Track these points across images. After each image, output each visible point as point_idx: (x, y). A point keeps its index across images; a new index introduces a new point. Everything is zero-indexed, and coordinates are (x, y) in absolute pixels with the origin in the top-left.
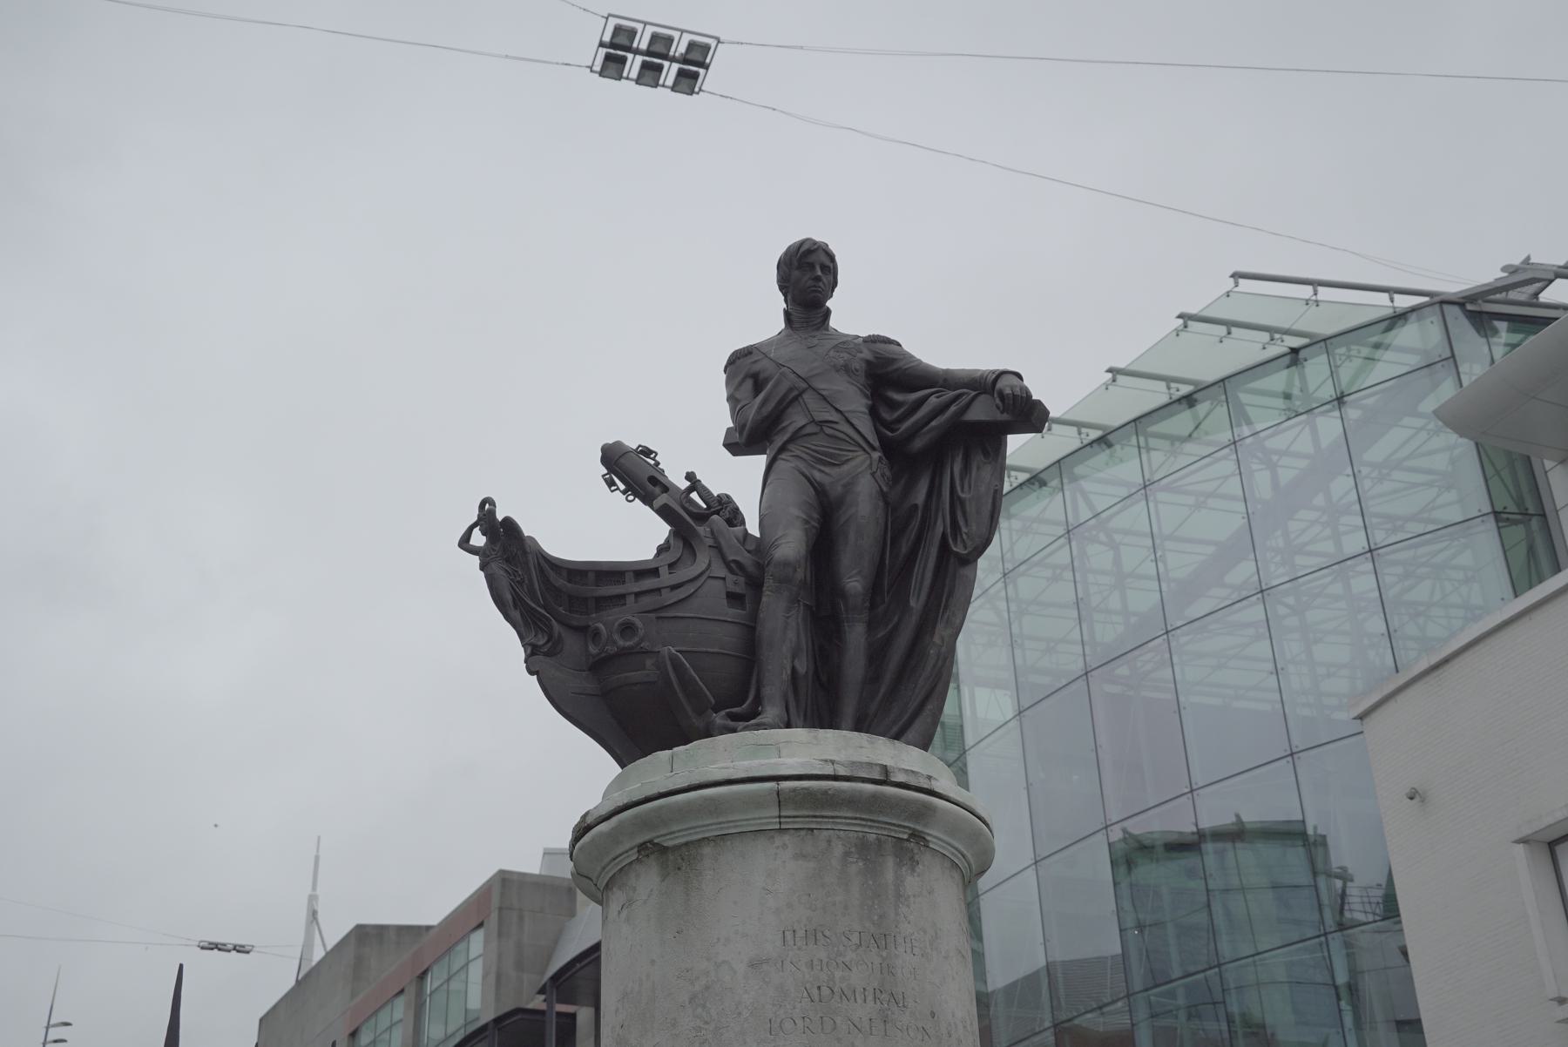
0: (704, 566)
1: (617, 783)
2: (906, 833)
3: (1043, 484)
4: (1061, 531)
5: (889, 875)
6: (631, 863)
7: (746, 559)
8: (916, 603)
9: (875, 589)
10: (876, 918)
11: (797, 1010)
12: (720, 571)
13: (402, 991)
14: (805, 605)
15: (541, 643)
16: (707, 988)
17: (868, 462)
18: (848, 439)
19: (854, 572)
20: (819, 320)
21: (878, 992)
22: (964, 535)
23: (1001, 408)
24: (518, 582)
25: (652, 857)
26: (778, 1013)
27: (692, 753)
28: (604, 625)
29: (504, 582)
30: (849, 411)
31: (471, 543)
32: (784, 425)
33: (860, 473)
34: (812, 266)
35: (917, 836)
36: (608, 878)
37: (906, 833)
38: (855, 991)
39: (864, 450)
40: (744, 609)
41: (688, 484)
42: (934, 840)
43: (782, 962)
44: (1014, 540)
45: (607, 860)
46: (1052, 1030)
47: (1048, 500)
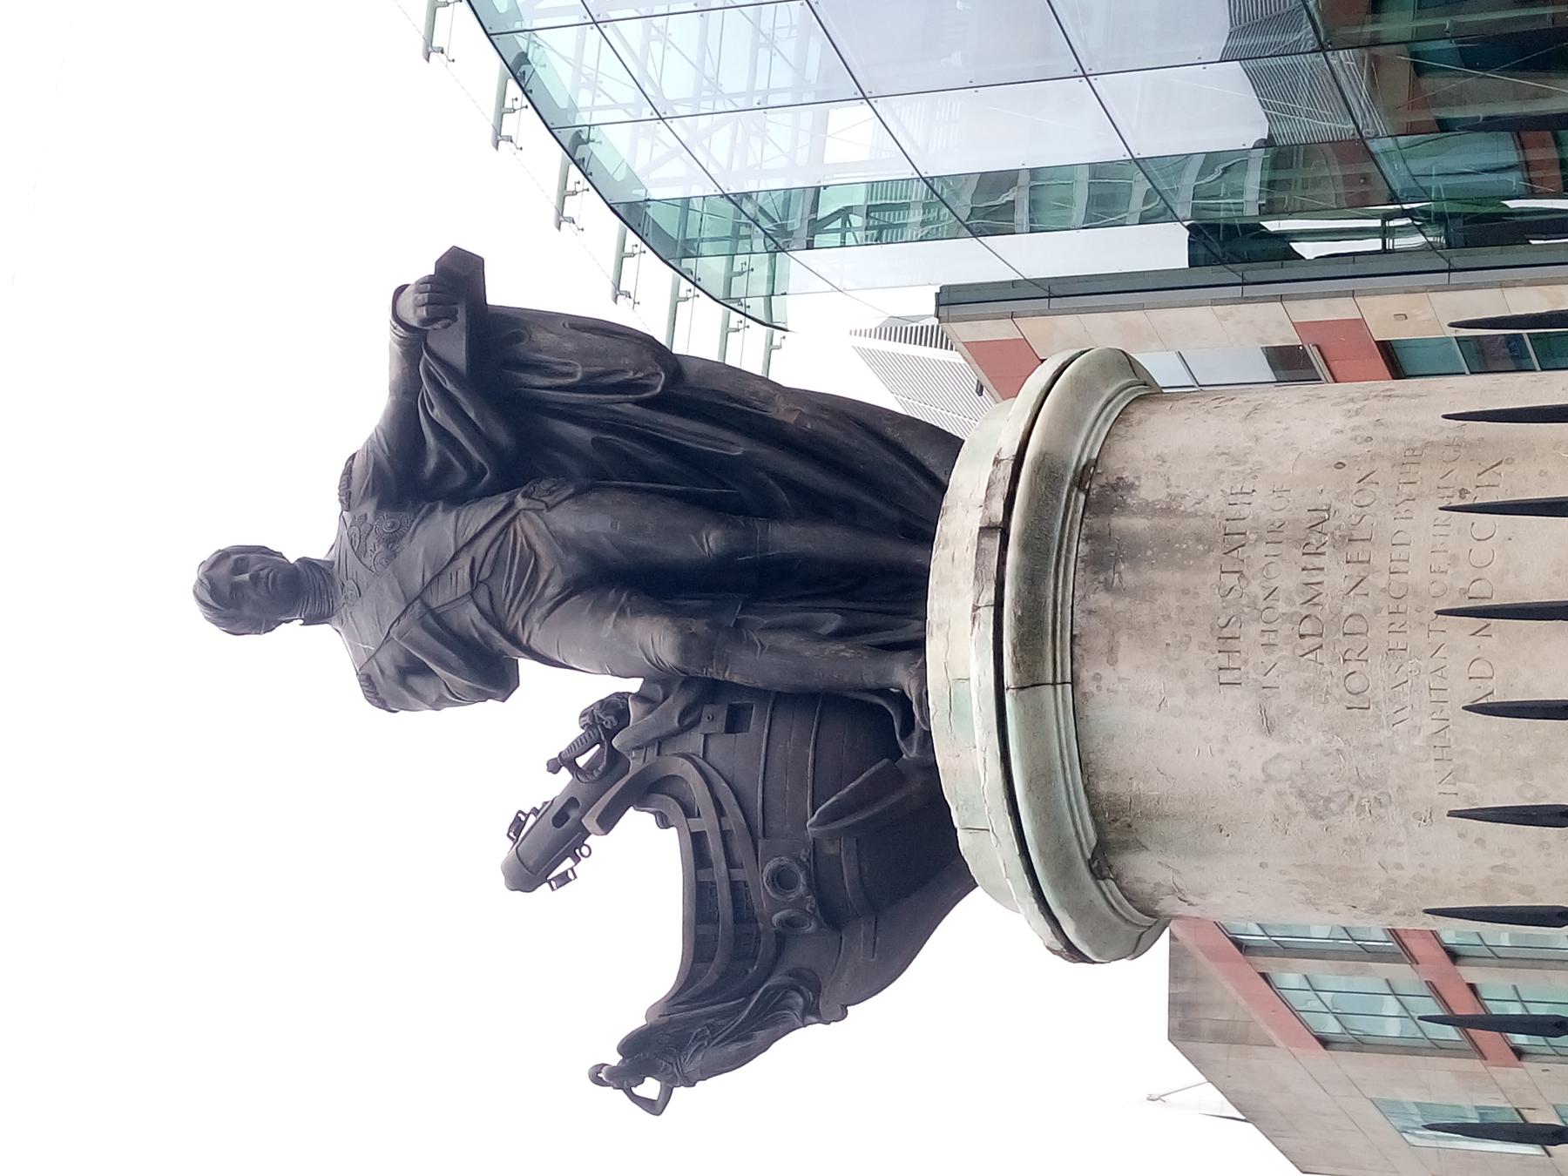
0: (688, 765)
1: (999, 895)
2: (1077, 497)
3: (523, 58)
4: (593, 34)
5: (1138, 524)
6: (1121, 889)
7: (675, 705)
8: (738, 447)
9: (717, 508)
10: (1200, 547)
11: (1334, 670)
12: (695, 741)
13: (1264, 976)
14: (742, 611)
15: (800, 1000)
16: (1301, 795)
17: (533, 516)
18: (498, 544)
20: (318, 576)
21: (1308, 549)
22: (639, 375)
23: (448, 321)
25: (1112, 861)
26: (1337, 697)
27: (961, 803)
28: (774, 914)
29: (715, 1054)
30: (456, 541)
31: (656, 1098)
32: (477, 636)
33: (547, 526)
34: (236, 587)
35: (1082, 479)
36: (1141, 915)
37: (1077, 496)
38: (1306, 584)
39: (513, 519)
41: (564, 770)
42: (1087, 450)
43: (1264, 688)
44: (610, 102)
45: (1115, 919)
46: (1329, 54)
47: (548, 52)
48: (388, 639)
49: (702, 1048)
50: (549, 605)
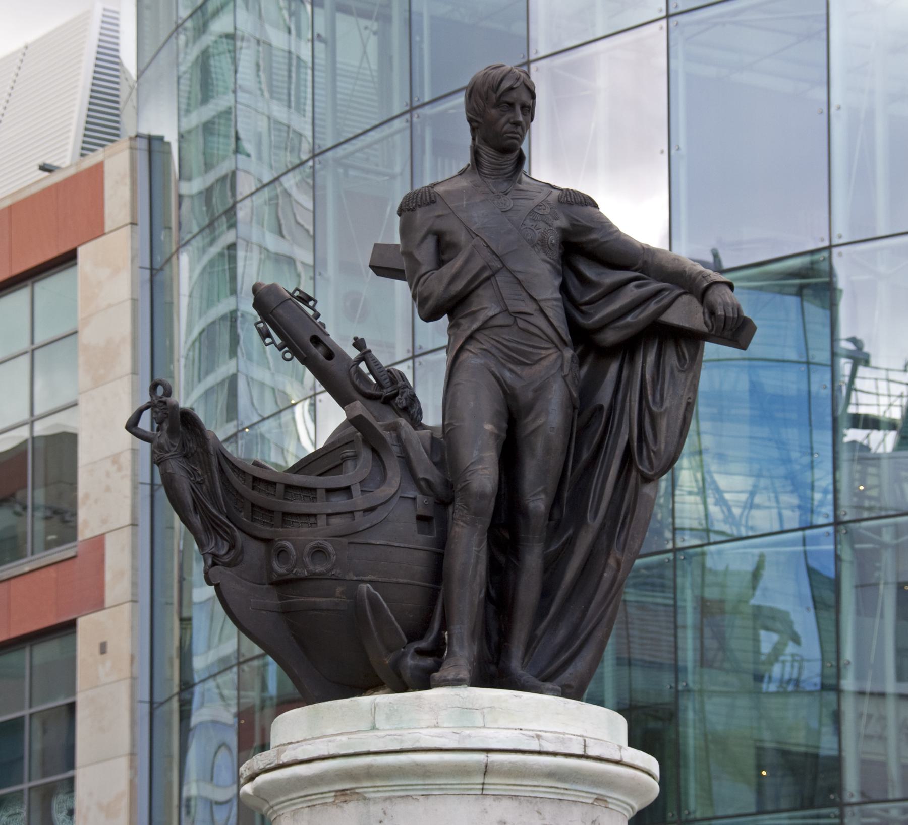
2: (590, 798)
19: (540, 489)
24: (198, 483)
27: (396, 707)
28: (292, 544)
32: (474, 309)
40: (430, 533)
48: (474, 235)
49: (188, 475)
50: (497, 373)
